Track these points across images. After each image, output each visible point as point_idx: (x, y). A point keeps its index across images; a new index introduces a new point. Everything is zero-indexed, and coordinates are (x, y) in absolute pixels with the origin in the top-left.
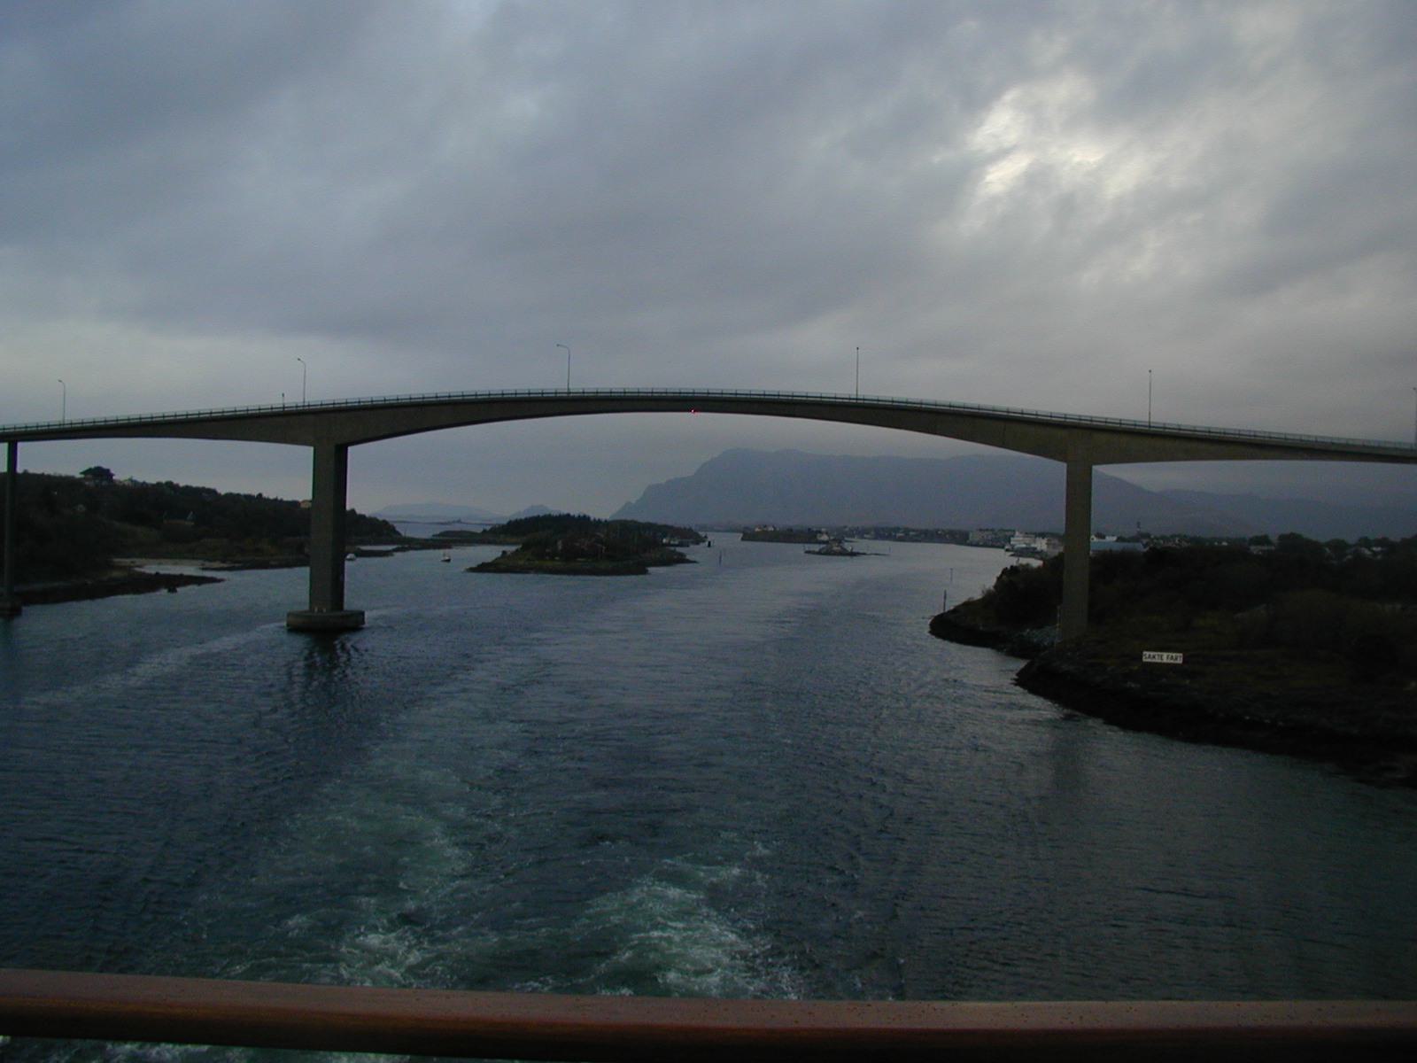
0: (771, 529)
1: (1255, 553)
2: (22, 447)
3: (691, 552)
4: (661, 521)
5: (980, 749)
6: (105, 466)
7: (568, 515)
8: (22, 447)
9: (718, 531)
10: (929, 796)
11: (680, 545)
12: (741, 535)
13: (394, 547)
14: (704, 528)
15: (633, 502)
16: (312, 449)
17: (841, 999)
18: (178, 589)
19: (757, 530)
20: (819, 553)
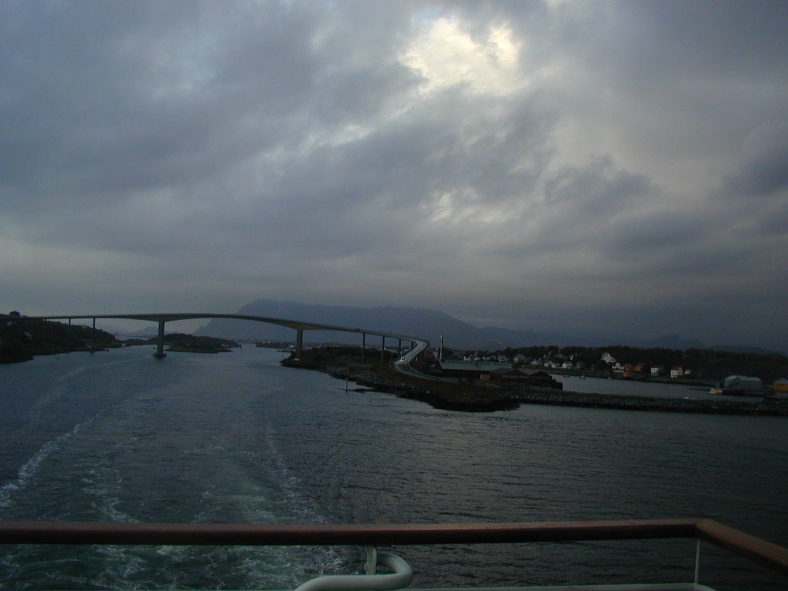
0: (269, 342)
1: (608, 362)
2: (72, 320)
3: (233, 349)
4: (221, 337)
5: (499, 419)
6: (17, 311)
7: (184, 334)
8: (72, 320)
9: (248, 343)
10: (443, 479)
11: (228, 347)
12: (256, 345)
13: (371, 388)
14: (241, 341)
15: (204, 326)
16: (158, 323)
17: (454, 523)
18: (34, 357)
19: (263, 342)
20: (282, 351)
